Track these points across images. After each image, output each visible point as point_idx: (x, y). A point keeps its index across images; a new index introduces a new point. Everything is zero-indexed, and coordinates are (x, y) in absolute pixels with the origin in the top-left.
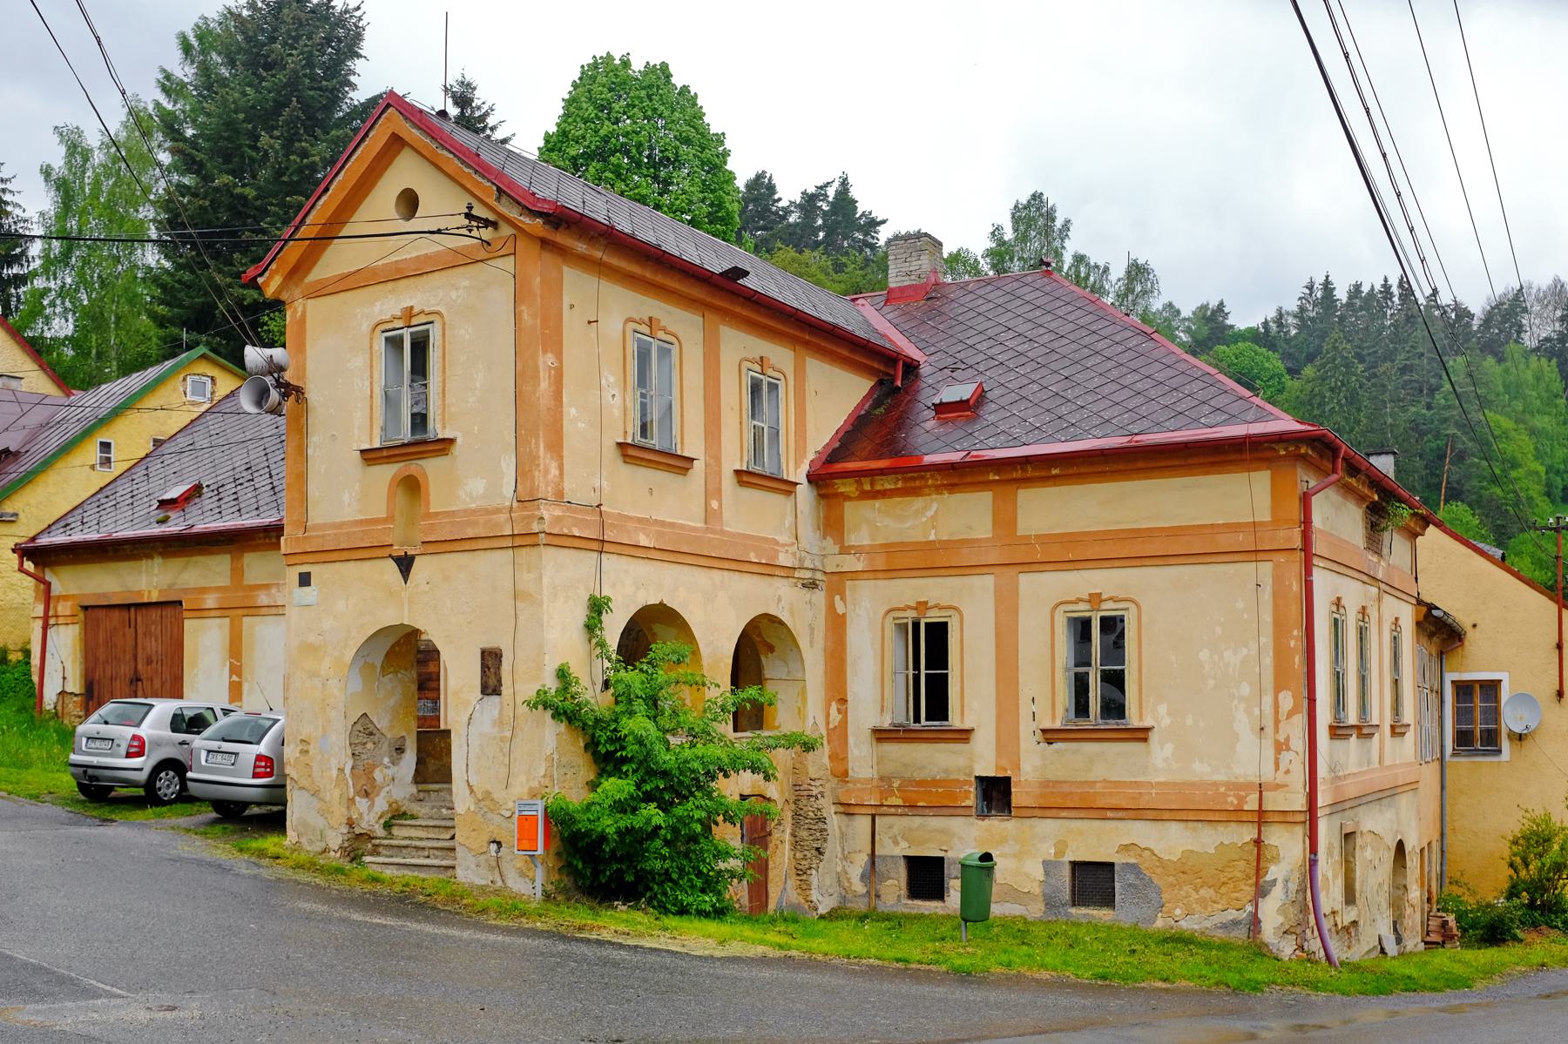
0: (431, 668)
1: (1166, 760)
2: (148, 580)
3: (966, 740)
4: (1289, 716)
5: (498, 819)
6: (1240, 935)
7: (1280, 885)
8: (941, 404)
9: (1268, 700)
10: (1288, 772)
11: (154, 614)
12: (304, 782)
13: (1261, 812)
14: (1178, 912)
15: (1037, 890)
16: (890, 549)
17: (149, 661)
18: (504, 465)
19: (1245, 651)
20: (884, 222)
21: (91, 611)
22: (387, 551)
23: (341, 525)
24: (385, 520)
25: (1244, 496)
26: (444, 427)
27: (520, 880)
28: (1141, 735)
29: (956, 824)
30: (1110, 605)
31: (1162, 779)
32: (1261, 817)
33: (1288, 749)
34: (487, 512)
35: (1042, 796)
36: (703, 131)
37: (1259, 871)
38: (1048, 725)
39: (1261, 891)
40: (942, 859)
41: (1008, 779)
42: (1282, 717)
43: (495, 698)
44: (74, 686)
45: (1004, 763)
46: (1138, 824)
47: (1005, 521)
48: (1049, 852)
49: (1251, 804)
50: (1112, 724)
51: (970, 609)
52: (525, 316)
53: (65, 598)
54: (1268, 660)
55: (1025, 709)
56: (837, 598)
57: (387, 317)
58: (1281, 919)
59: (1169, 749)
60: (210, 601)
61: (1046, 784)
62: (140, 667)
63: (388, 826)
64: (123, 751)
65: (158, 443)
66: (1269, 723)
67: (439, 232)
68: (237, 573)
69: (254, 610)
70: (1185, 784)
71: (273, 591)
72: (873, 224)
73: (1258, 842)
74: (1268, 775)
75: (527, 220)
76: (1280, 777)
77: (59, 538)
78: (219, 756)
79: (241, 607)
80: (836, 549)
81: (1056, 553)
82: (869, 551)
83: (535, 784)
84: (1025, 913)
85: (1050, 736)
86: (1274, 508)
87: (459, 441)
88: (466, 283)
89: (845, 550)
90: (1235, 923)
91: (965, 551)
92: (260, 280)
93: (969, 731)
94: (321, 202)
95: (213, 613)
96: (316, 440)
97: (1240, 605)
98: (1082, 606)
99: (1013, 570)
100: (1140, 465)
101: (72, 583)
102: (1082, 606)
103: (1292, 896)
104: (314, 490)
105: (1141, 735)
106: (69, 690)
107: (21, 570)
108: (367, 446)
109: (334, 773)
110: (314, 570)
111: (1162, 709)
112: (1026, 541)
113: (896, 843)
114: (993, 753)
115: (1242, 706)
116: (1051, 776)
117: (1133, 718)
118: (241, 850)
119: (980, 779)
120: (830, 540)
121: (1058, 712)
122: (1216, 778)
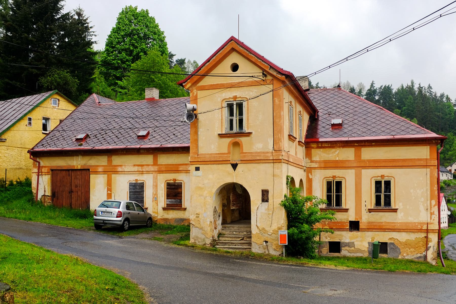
0: (179, 190)
1: (402, 217)
2: (77, 163)
3: (347, 212)
4: (434, 206)
5: (267, 235)
6: (422, 260)
7: (432, 248)
8: (334, 124)
9: (429, 202)
10: (434, 220)
11: (78, 173)
12: (196, 225)
13: (427, 230)
14: (405, 254)
15: (366, 250)
16: (325, 162)
17: (76, 186)
18: (269, 141)
19: (422, 190)
20: (175, 55)
21: (54, 172)
22: (229, 162)
23: (211, 154)
24: (227, 154)
25: (423, 152)
26: (248, 129)
27: (274, 251)
28: (395, 210)
29: (344, 233)
30: (387, 178)
31: (401, 222)
32: (427, 231)
33: (434, 214)
34: (264, 153)
35: (368, 226)
36: (159, 31)
37: (427, 244)
38: (370, 208)
39: (427, 249)
40: (340, 242)
41: (359, 222)
42: (432, 206)
43: (267, 203)
44: (48, 193)
45: (357, 217)
46: (394, 233)
47: (358, 156)
48: (370, 240)
49: (425, 227)
50: (387, 208)
51: (348, 178)
52: (276, 101)
53: (45, 167)
54: (429, 193)
55: (363, 204)
56: (310, 174)
57: (228, 97)
58: (432, 256)
59: (402, 214)
60: (100, 169)
61: (369, 223)
62: (73, 188)
63: (218, 237)
64: (116, 216)
65: (61, 121)
66: (429, 208)
67: (252, 77)
68: (110, 161)
69: (116, 172)
70: (407, 223)
71: (123, 167)
72: (171, 56)
73: (427, 237)
74: (429, 221)
75: (280, 76)
76: (432, 221)
77: (40, 149)
78: (106, 213)
79: (111, 171)
80: (309, 161)
81: (372, 164)
82: (319, 162)
83: (280, 226)
84: (363, 255)
85: (370, 211)
86: (430, 155)
87: (253, 133)
88: (256, 91)
89: (312, 162)
90: (420, 257)
91: (347, 163)
92: (184, 84)
93: (348, 209)
94: (207, 64)
95: (101, 173)
96: (201, 131)
97: (421, 179)
98: (379, 178)
99: (360, 168)
100: (396, 143)
101: (46, 162)
102: (379, 178)
103: (435, 250)
104: (200, 144)
105: (395, 210)
106: (46, 194)
107: (30, 158)
108: (220, 133)
109: (209, 223)
110: (201, 167)
111: (401, 204)
112: (364, 161)
113: (326, 238)
114: (354, 215)
115: (422, 204)
116: (370, 221)
117: (393, 206)
118: (60, 239)
119: (350, 222)
120: (307, 159)
121: (372, 204)
122: (415, 221)
